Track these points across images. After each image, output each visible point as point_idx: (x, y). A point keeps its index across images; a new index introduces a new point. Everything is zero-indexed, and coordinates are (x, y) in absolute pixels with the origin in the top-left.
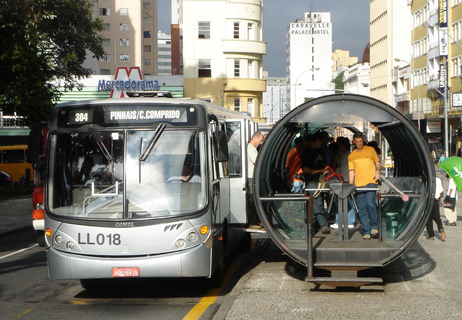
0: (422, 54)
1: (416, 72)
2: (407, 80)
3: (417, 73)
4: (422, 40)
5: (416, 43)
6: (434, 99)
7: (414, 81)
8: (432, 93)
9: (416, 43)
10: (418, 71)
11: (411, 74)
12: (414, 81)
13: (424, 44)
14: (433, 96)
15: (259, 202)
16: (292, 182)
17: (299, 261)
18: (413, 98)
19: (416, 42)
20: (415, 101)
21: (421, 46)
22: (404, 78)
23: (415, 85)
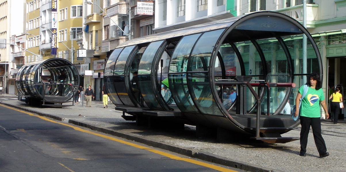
0: (35, 28)
1: (30, 39)
2: (23, 44)
3: (31, 39)
4: (35, 19)
5: (30, 21)
6: (44, 55)
7: (28, 44)
8: (43, 51)
9: (30, 21)
10: (32, 38)
11: (26, 40)
12: (28, 44)
13: (37, 22)
14: (44, 54)
15: (214, 84)
16: (28, 91)
17: (239, 126)
18: (27, 55)
19: (30, 20)
20: (29, 57)
21: (37, 22)
22: (20, 43)
23: (29, 47)
